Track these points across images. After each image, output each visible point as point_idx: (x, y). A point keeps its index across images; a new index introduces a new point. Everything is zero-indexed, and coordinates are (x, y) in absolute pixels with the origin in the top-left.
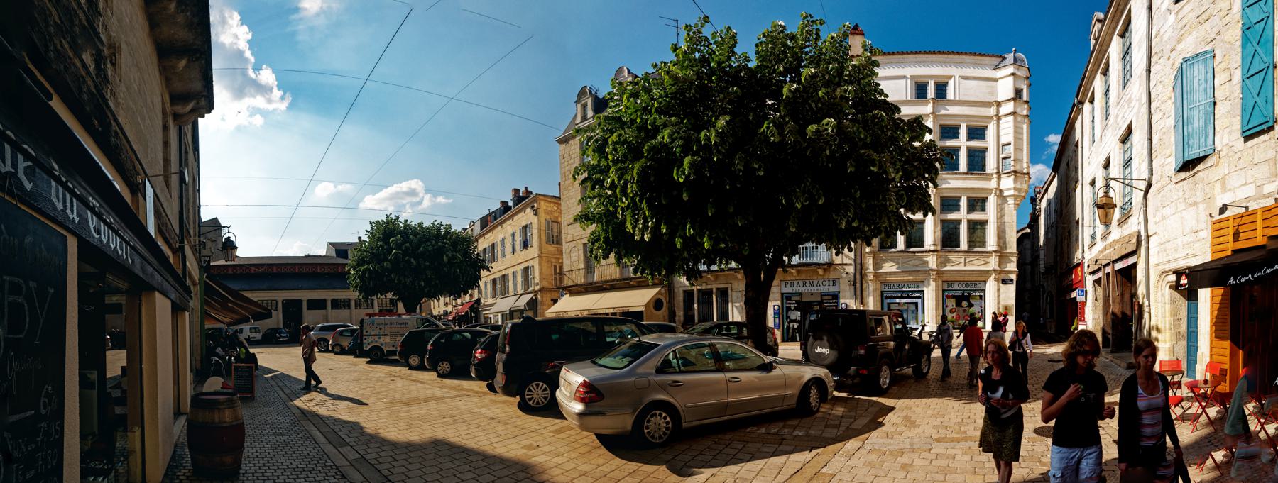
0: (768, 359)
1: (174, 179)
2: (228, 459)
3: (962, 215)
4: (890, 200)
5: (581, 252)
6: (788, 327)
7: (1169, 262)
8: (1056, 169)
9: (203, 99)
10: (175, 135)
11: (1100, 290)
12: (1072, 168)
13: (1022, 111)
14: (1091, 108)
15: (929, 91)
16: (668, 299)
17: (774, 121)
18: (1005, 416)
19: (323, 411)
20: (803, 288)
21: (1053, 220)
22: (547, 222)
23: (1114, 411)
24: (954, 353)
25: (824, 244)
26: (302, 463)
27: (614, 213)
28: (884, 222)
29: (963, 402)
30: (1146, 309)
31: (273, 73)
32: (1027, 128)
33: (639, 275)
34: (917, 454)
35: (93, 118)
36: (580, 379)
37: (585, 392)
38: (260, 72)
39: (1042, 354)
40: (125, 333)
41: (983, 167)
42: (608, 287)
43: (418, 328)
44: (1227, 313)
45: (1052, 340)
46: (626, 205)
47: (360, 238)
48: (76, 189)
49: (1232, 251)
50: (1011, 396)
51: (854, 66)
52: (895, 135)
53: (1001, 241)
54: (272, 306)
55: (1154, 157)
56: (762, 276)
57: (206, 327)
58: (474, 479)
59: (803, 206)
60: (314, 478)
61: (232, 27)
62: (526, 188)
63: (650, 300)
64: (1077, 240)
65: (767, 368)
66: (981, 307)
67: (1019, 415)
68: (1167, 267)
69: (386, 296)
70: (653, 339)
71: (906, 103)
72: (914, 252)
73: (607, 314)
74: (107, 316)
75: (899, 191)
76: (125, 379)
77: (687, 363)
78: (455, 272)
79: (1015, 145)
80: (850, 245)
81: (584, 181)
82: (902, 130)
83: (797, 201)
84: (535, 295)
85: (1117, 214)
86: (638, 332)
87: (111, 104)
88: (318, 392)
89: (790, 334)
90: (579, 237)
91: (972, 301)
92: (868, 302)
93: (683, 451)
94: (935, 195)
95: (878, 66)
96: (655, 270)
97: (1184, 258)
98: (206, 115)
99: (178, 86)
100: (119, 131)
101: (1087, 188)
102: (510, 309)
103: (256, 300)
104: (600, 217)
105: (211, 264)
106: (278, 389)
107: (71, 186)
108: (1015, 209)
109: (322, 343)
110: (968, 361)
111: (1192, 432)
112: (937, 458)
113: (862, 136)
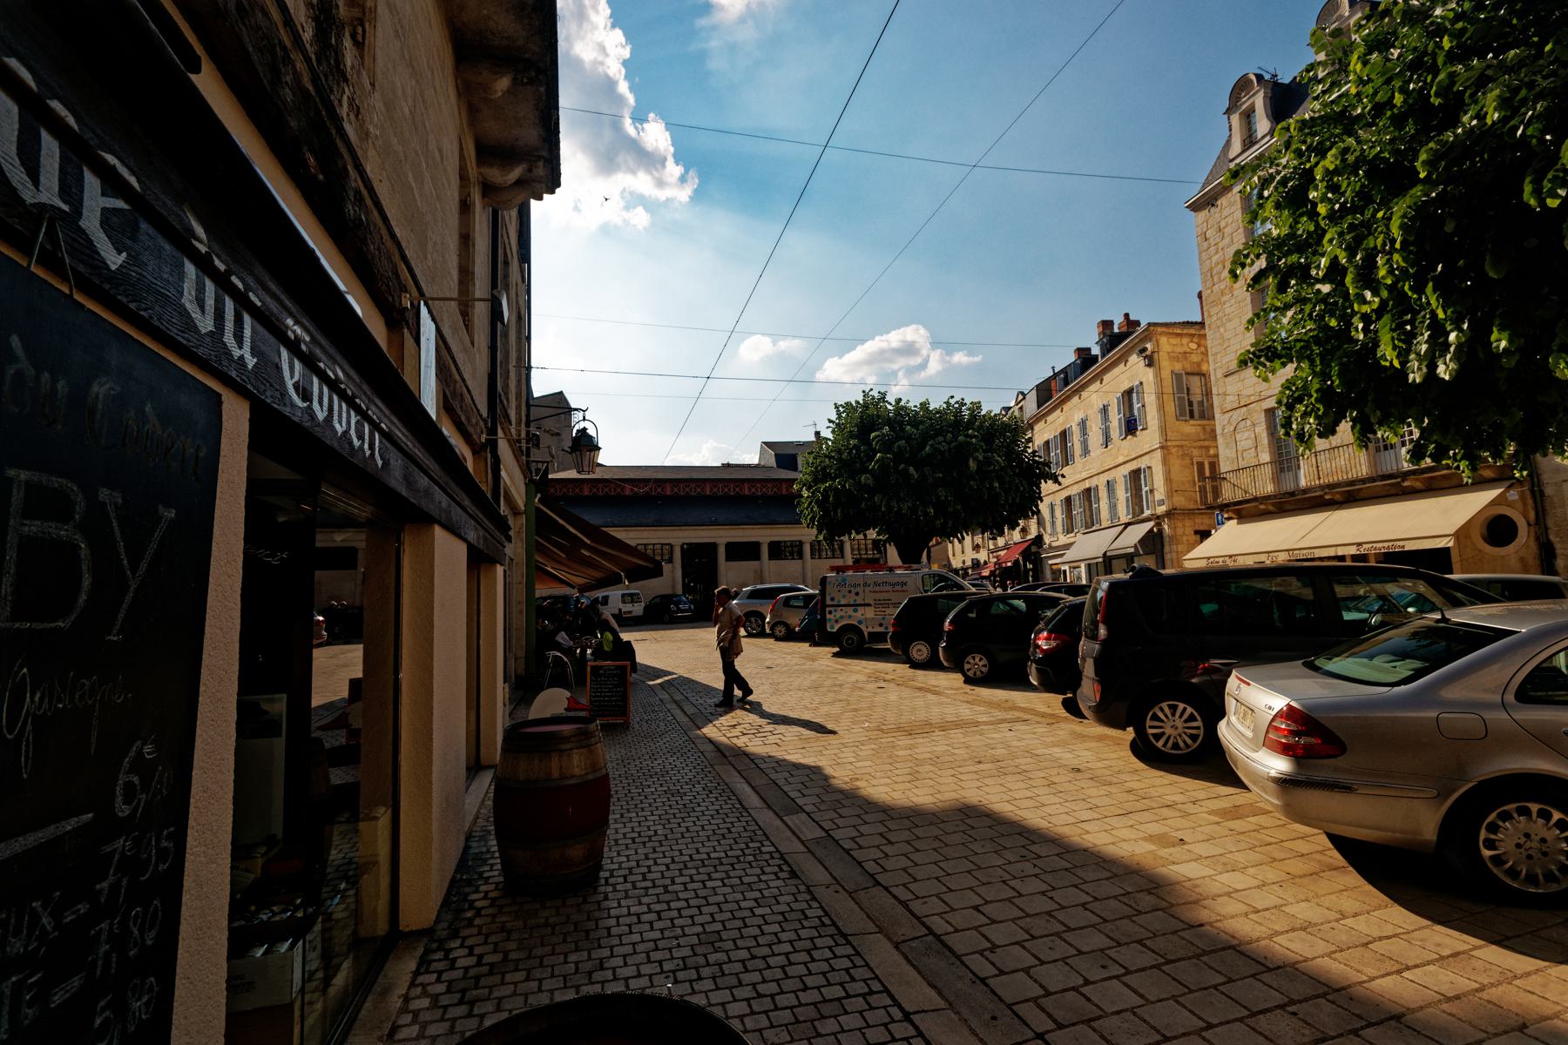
1: (481, 311)
2: (577, 852)
5: (1262, 430)
9: (541, 164)
10: (485, 224)
16: (1532, 514)
19: (755, 746)
22: (1177, 377)
26: (718, 848)
27: (1344, 334)
31: (667, 129)
33: (1428, 462)
35: (305, 149)
36: (1279, 702)
37: (1293, 733)
38: (645, 125)
40: (361, 608)
42: (1338, 497)
43: (926, 591)
46: (1375, 306)
47: (817, 434)
48: (251, 294)
54: (662, 554)
57: (538, 594)
58: (1043, 893)
60: (740, 878)
61: (595, 27)
62: (1127, 316)
69: (865, 536)
70: (1490, 617)
73: (1342, 558)
74: (318, 573)
76: (359, 705)
78: (992, 488)
81: (1257, 279)
84: (1158, 524)
86: (1437, 600)
87: (349, 129)
88: (746, 710)
90: (1253, 399)
96: (1482, 447)
98: (545, 196)
99: (494, 130)
100: (364, 192)
102: (1105, 553)
103: (632, 543)
104: (1307, 346)
105: (550, 476)
106: (674, 706)
107: (240, 286)
109: (753, 619)
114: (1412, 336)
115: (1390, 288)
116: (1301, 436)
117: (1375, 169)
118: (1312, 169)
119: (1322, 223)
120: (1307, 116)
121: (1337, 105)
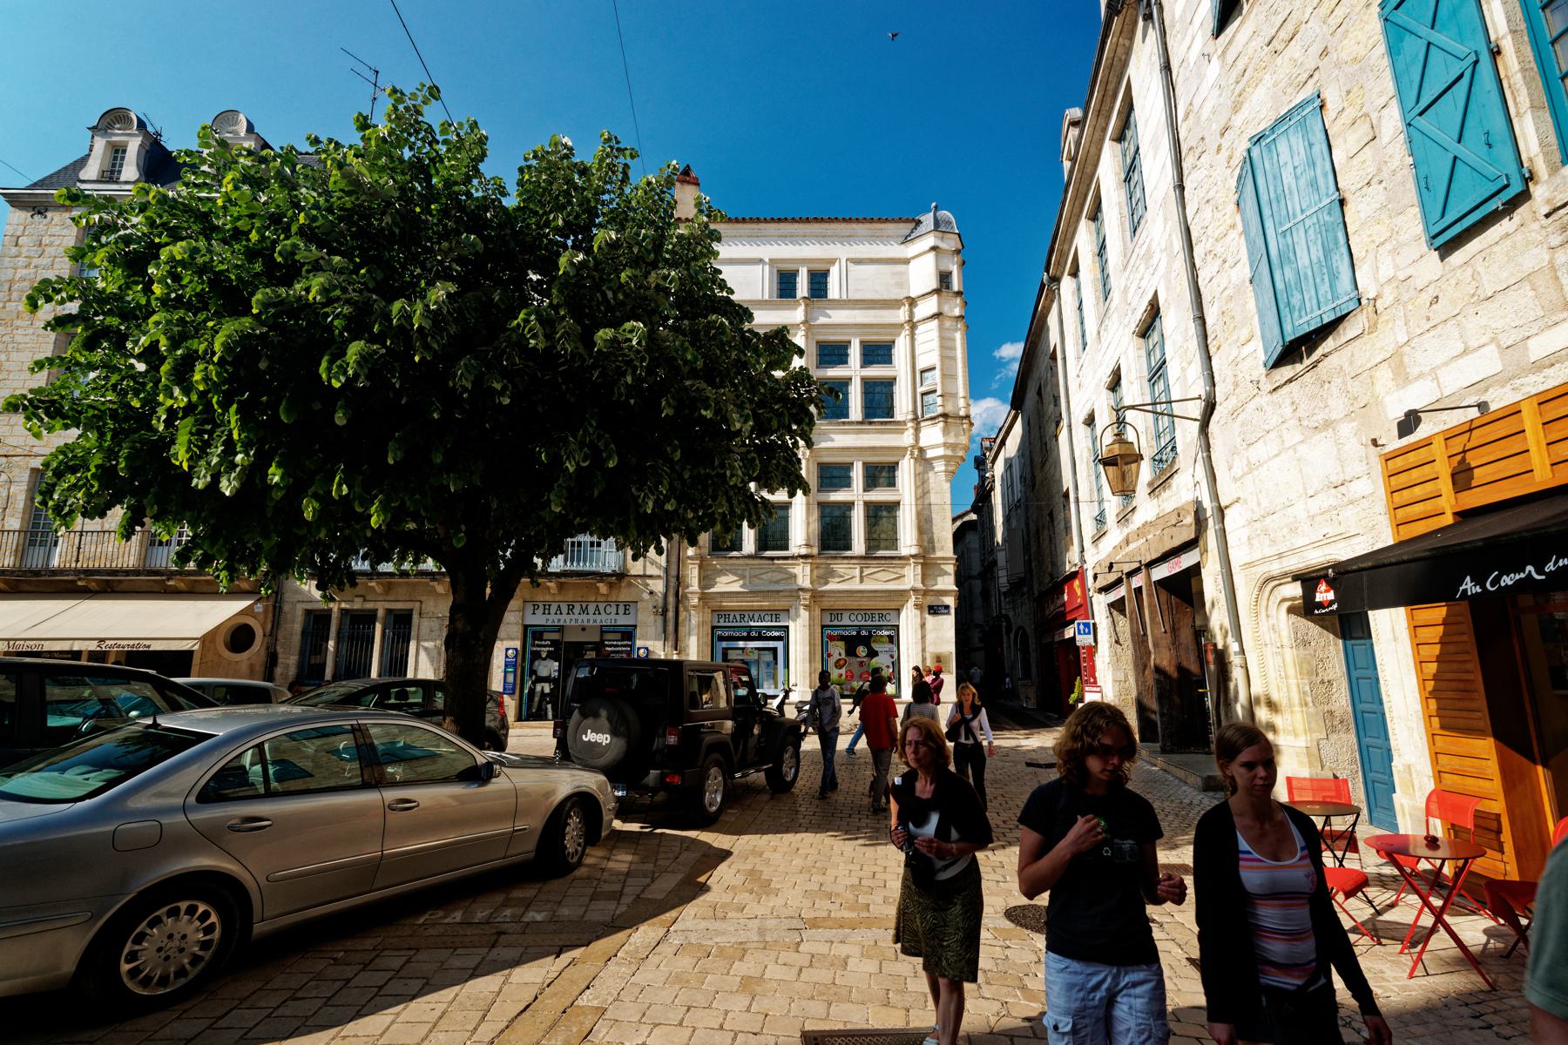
0: (482, 757)
3: (856, 494)
4: (732, 468)
6: (532, 691)
7: (1280, 556)
8: (1017, 404)
11: (1124, 624)
12: (1047, 398)
13: (952, 311)
14: (1074, 286)
15: (799, 286)
16: (269, 626)
17: (538, 311)
18: (944, 876)
20: (568, 618)
21: (1018, 495)
23: (1182, 887)
24: (843, 743)
25: (612, 539)
27: (143, 419)
28: (721, 505)
29: (861, 842)
30: (1235, 660)
32: (962, 339)
34: (773, 955)
39: (1012, 749)
41: (889, 411)
42: (93, 586)
44: (1469, 666)
45: (1031, 722)
46: (182, 405)
49: (1455, 514)
50: (954, 834)
51: (680, 237)
52: (743, 359)
53: (926, 537)
55: (1212, 350)
56: (488, 591)
59: (579, 468)
63: (218, 627)
64: (1068, 528)
65: (479, 775)
66: (892, 657)
67: (972, 876)
68: (1276, 568)
71: (763, 304)
72: (772, 559)
73: (76, 655)
75: (749, 452)
77: (288, 771)
79: (942, 370)
80: (660, 542)
81: (60, 322)
82: (756, 350)
83: (568, 458)
85: (1145, 472)
86: (160, 703)
89: (535, 704)
90: (19, 451)
91: (875, 646)
92: (687, 646)
93: (242, 1000)
94: (808, 460)
95: (719, 240)
96: (241, 562)
97: (1316, 545)
101: (1081, 431)
104: (100, 417)
108: (947, 481)
110: (870, 759)
111: (1411, 976)
112: (811, 965)
113: (689, 357)
114: (207, 444)
115: (202, 395)
116: (58, 509)
117: (218, 282)
118: (160, 246)
119: (154, 303)
120: (170, 194)
121: (203, 205)
